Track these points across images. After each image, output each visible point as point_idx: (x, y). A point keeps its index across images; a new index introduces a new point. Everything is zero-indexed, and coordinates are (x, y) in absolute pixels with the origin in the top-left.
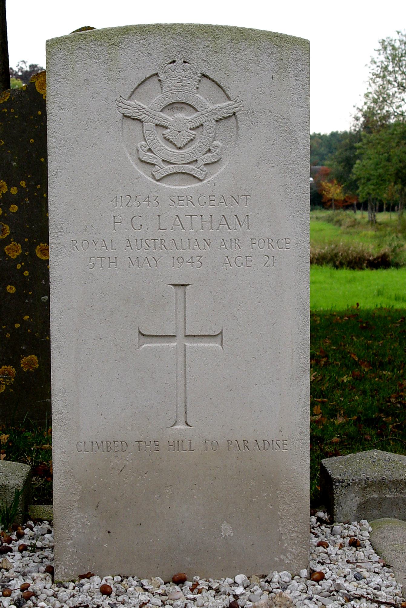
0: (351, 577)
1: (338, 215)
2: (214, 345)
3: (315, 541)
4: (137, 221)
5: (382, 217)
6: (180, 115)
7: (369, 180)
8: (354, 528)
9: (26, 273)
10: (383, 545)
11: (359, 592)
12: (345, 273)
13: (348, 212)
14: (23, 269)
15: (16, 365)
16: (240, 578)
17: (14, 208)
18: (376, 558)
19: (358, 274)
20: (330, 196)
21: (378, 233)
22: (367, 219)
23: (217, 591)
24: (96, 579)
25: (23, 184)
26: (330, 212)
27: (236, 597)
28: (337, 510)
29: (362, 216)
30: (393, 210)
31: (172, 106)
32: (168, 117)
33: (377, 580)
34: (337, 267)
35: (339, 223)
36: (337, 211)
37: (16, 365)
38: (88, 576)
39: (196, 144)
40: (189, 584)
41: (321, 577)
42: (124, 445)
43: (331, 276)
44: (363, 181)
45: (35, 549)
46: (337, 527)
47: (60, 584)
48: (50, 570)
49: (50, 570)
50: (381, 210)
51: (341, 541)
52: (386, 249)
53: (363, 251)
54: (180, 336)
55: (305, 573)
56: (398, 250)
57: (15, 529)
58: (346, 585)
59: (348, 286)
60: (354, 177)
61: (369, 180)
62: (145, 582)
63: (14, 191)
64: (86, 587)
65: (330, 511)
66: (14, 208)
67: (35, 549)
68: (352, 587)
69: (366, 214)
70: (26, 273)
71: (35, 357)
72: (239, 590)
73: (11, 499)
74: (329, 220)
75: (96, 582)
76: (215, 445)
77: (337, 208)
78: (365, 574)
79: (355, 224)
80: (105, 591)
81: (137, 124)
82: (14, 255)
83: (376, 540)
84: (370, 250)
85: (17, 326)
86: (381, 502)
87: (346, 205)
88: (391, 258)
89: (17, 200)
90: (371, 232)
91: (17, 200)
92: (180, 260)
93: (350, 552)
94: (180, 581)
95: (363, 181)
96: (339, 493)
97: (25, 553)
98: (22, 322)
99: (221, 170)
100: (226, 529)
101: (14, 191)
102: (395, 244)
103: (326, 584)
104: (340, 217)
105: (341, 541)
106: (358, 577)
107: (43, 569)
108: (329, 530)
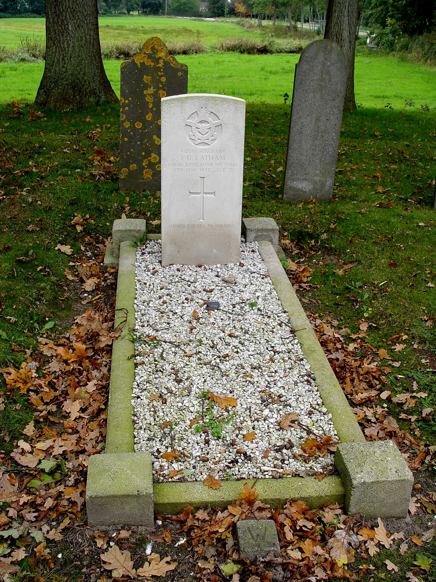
0: (252, 265)
1: (243, 21)
2: (213, 196)
3: (241, 250)
4: (189, 157)
5: (265, 23)
6: (204, 125)
7: (259, 4)
8: (253, 244)
9: (132, 133)
10: (262, 252)
11: (254, 271)
12: (246, 56)
13: (247, 19)
14: (131, 132)
15: (128, 168)
16: (219, 265)
17: (127, 108)
18: (260, 257)
19: (252, 57)
20: (239, 11)
21: (263, 32)
22: (257, 24)
23: (212, 269)
24: (175, 265)
25: (130, 99)
26: (239, 19)
27: (218, 272)
28: (248, 238)
29: (254, 21)
30: (270, 19)
31: (201, 122)
32: (200, 125)
33: (260, 266)
34: (242, 52)
35: (243, 25)
36: (242, 19)
37: (128, 168)
38: (172, 265)
39: (208, 134)
40: (203, 267)
41: (243, 265)
42: (184, 226)
43: (239, 58)
44: (256, 5)
45: (153, 253)
46: (248, 244)
47: (164, 267)
48: (160, 262)
49: (160, 262)
50: (264, 19)
51: (249, 249)
52: (266, 43)
53: (255, 44)
54: (202, 193)
55: (238, 264)
56: (272, 44)
57: (144, 244)
58: (250, 268)
59: (247, 64)
60: (252, 3)
61: (259, 4)
62: (190, 266)
63: (127, 102)
64: (172, 268)
65: (245, 238)
66: (127, 108)
67: (153, 253)
68: (252, 269)
69: (257, 20)
70: (132, 133)
71: (135, 165)
72: (219, 270)
73: (142, 234)
74: (238, 23)
75: (175, 267)
76: (212, 226)
77: (242, 17)
78: (256, 264)
79: (251, 26)
80: (178, 270)
81: (190, 128)
82: (127, 126)
83: (260, 250)
84: (258, 44)
85: (128, 153)
86: (261, 236)
87: (247, 16)
88: (268, 48)
89: (128, 105)
90: (259, 32)
91: (128, 105)
92: (203, 170)
93: (252, 254)
94: (200, 266)
95: (256, 5)
96: (248, 233)
97: (150, 255)
98: (130, 152)
99: (216, 142)
100: (215, 251)
101: (127, 102)
102: (270, 40)
103: (245, 268)
104: (243, 22)
105: (249, 249)
106: (254, 265)
107: (157, 261)
108: (245, 245)
